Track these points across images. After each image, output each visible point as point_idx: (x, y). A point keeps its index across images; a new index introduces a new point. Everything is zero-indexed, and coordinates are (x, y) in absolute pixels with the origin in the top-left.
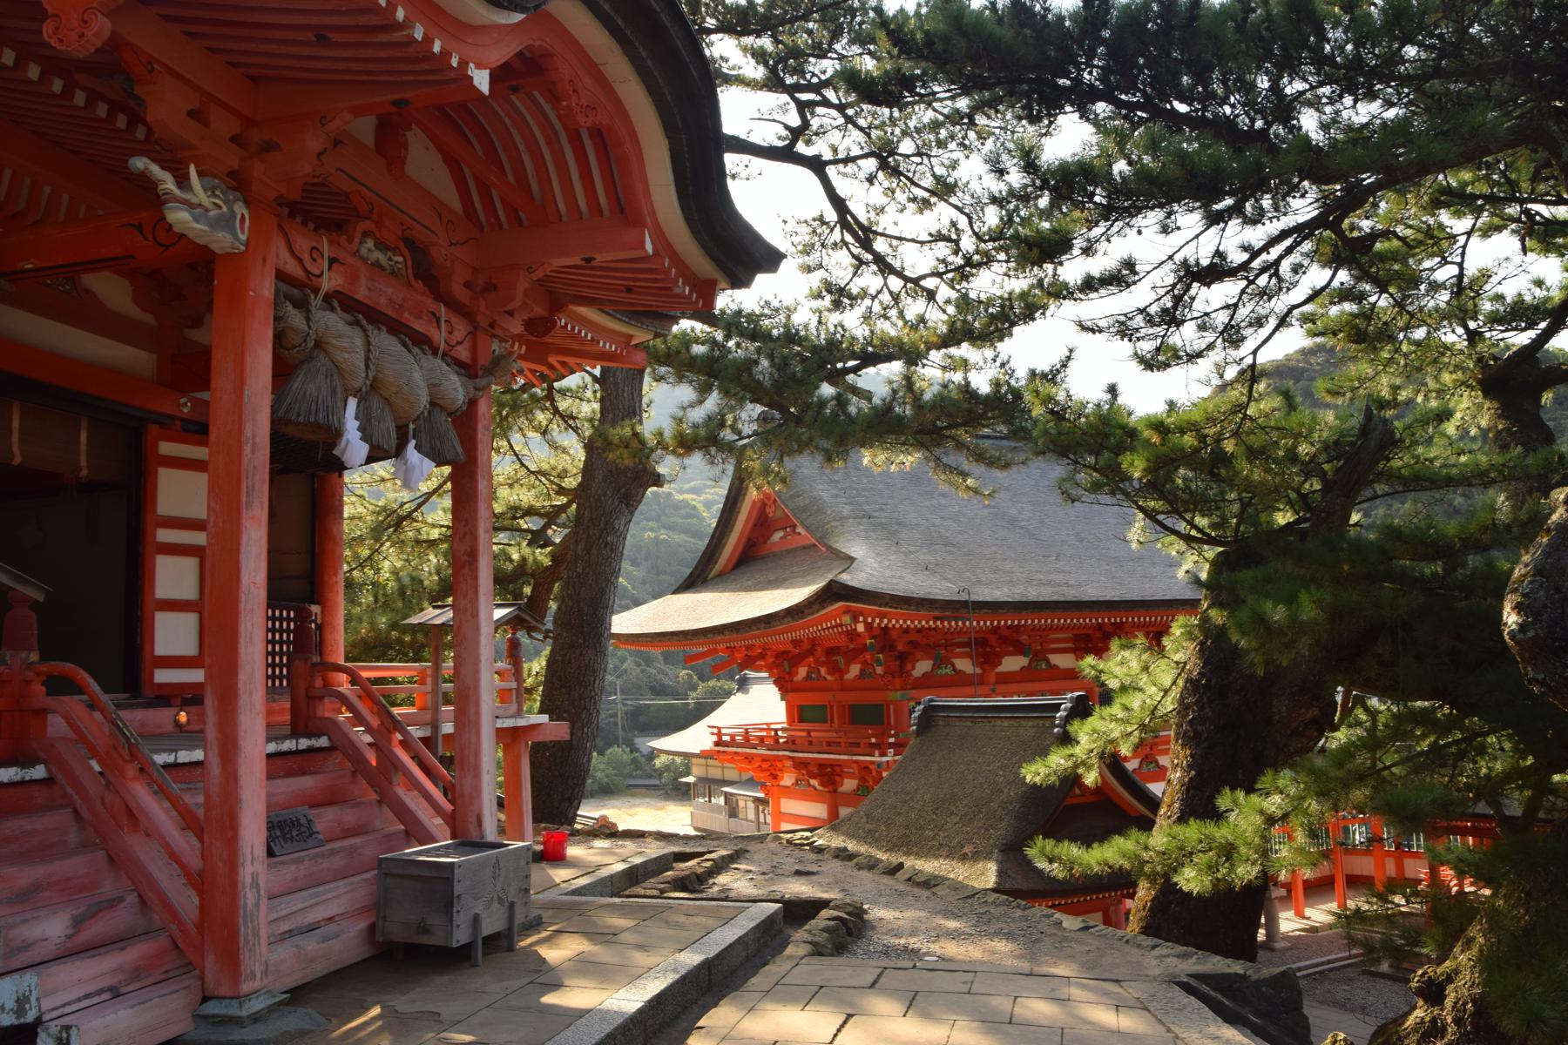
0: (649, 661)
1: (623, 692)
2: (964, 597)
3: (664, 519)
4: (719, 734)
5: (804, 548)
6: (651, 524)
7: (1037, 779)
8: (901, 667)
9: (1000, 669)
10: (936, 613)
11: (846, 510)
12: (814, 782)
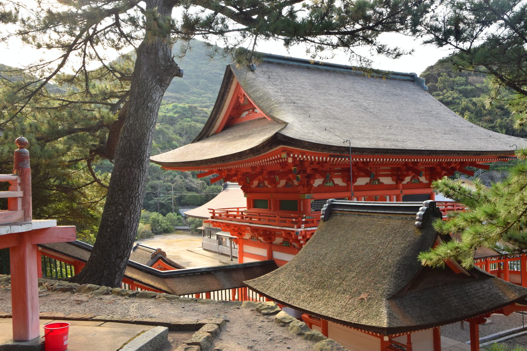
0: (186, 177)
1: (174, 189)
2: (347, 145)
3: (193, 117)
4: (214, 213)
5: (259, 119)
6: (188, 119)
7: (429, 263)
8: (308, 182)
9: (356, 184)
10: (332, 153)
11: (282, 99)
12: (261, 238)
